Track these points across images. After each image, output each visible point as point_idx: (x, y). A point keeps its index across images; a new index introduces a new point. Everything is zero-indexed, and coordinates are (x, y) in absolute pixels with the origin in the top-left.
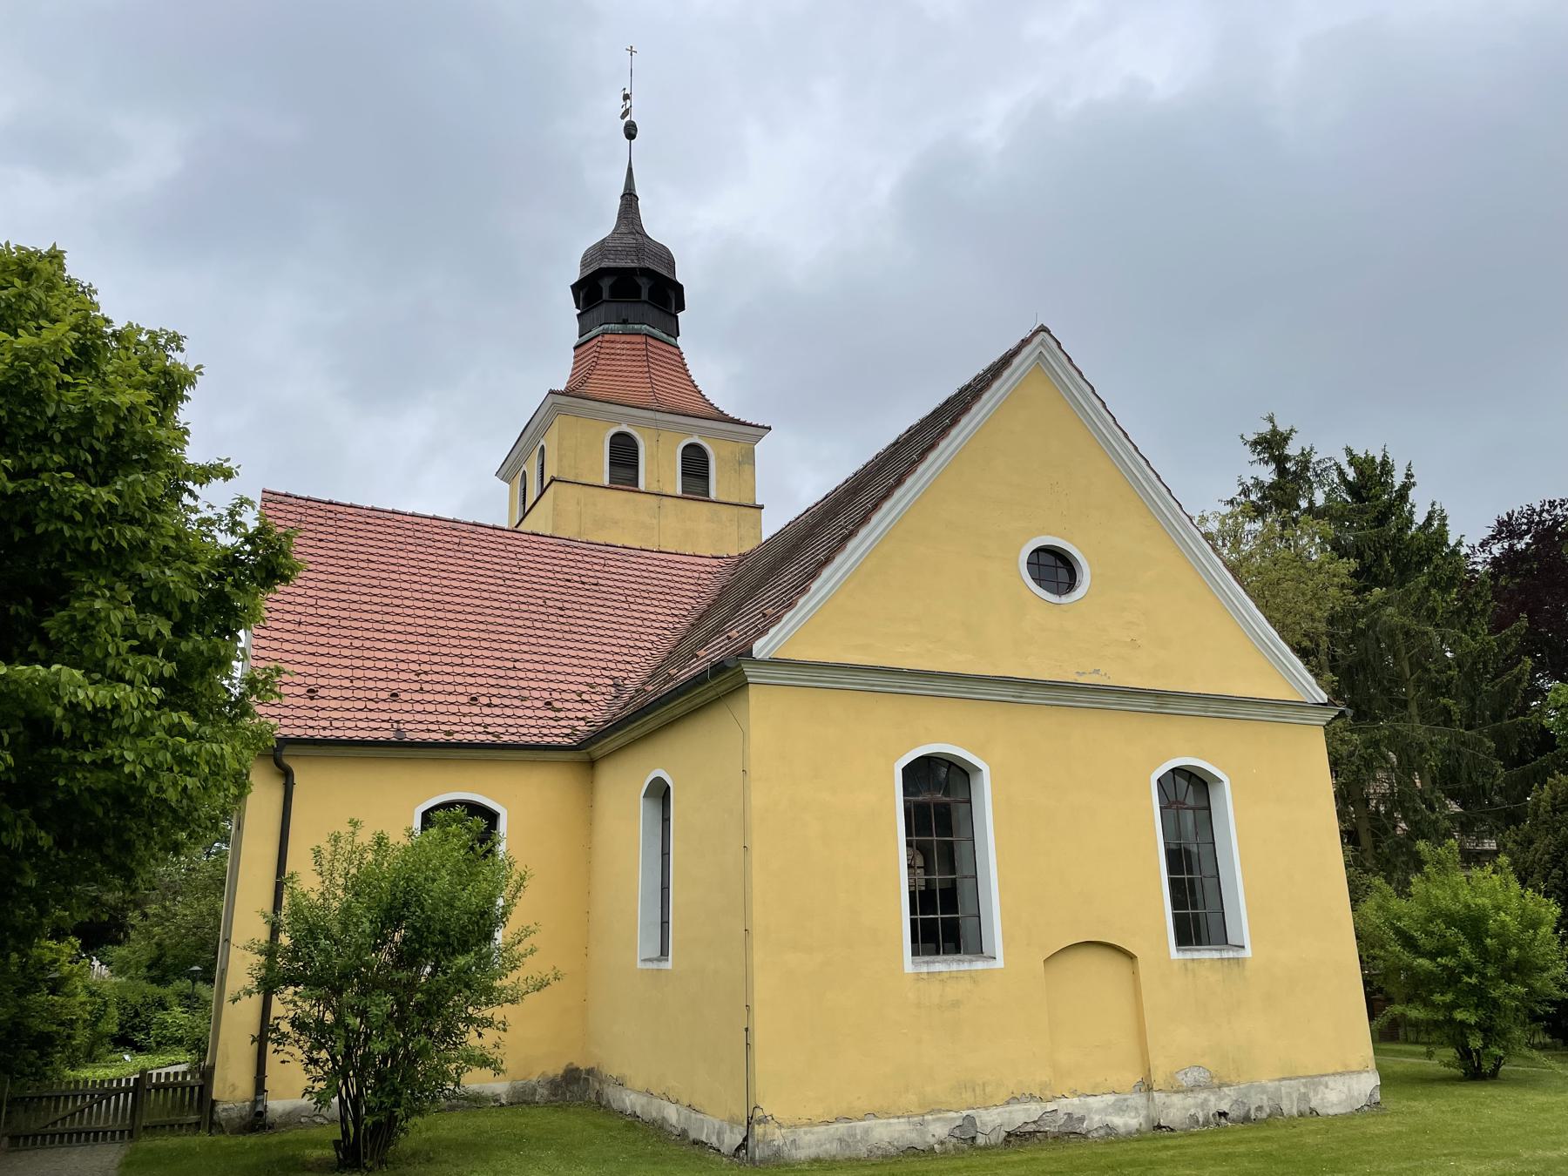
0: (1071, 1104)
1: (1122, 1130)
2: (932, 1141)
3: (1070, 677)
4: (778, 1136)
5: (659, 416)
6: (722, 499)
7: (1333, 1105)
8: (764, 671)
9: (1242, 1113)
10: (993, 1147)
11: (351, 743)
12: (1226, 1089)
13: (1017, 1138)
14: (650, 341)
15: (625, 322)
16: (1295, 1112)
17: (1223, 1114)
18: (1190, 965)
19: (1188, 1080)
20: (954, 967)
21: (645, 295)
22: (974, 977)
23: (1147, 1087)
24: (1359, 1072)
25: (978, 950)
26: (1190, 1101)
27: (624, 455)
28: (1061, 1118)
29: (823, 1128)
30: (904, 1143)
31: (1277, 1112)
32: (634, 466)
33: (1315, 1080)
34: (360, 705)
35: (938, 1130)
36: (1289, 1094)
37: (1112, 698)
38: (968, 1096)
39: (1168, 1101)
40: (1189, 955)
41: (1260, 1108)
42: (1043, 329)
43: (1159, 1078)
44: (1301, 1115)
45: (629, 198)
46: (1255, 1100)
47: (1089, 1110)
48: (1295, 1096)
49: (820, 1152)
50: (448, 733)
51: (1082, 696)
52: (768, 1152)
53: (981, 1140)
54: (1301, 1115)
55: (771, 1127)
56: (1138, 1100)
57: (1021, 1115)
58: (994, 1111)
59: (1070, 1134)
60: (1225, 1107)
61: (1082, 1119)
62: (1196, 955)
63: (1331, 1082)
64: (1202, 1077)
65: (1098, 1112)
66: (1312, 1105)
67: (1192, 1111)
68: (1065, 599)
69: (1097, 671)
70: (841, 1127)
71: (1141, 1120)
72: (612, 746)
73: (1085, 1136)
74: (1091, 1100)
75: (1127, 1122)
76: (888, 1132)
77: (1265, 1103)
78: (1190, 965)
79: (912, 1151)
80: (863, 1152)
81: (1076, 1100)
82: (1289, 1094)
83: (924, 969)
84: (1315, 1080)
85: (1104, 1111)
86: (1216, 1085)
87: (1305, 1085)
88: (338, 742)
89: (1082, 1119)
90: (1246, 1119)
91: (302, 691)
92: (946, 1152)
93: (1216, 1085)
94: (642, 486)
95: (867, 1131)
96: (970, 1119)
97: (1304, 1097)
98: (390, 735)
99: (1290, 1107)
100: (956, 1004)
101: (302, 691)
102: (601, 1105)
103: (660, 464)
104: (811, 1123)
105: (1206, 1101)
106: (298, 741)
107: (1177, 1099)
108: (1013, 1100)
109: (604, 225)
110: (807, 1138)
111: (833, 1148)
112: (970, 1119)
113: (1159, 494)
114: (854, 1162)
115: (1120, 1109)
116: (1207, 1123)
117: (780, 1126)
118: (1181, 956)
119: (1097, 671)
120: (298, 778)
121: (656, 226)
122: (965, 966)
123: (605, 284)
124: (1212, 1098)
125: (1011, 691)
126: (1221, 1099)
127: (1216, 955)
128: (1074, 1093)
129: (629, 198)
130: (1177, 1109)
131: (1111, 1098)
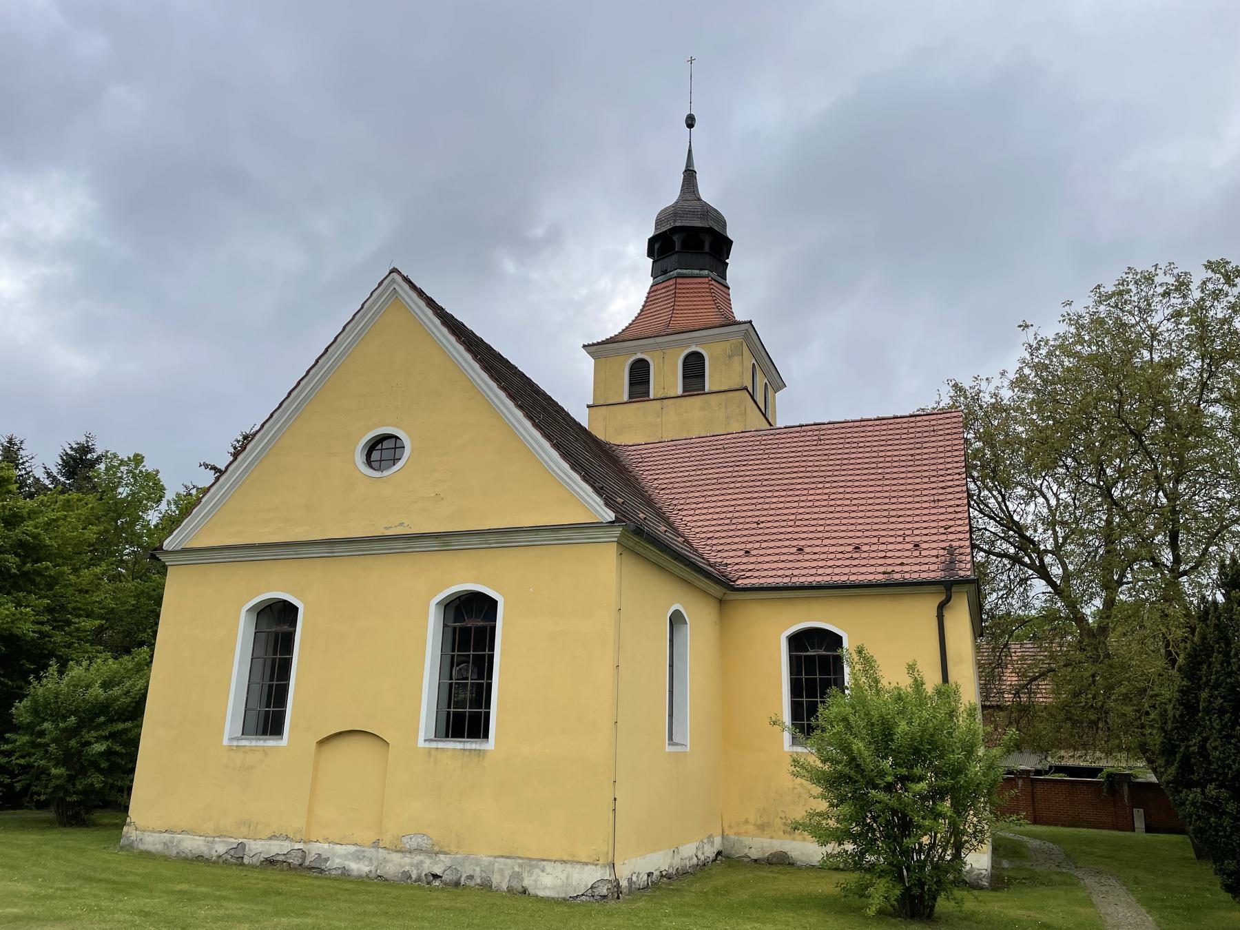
0: (322, 848)
1: (355, 873)
5: (658, 340)
6: (716, 389)
8: (171, 557)
12: (442, 857)
13: (271, 862)
14: (679, 280)
15: (665, 272)
16: (504, 886)
17: (436, 876)
19: (413, 844)
20: (254, 743)
21: (707, 249)
22: (265, 751)
23: (376, 844)
24: (587, 864)
25: (486, 736)
26: (407, 860)
27: (694, 369)
30: (197, 852)
31: (486, 886)
32: (647, 382)
33: (532, 863)
35: (221, 848)
36: (502, 871)
38: (244, 830)
39: (388, 857)
41: (471, 877)
42: (394, 270)
43: (387, 841)
45: (690, 175)
46: (467, 870)
47: (334, 854)
48: (507, 873)
51: (417, 543)
53: (246, 861)
54: (510, 890)
57: (276, 848)
58: (259, 843)
60: (438, 871)
61: (327, 860)
63: (549, 867)
64: (425, 843)
65: (340, 856)
66: (525, 883)
67: (407, 868)
69: (401, 524)
71: (373, 869)
72: (702, 585)
73: (321, 871)
75: (359, 867)
76: (192, 844)
77: (477, 874)
78: (433, 753)
79: (199, 858)
81: (326, 846)
82: (502, 871)
84: (532, 863)
85: (345, 857)
86: (432, 852)
87: (520, 866)
89: (327, 860)
90: (457, 884)
91: (794, 550)
93: (433, 852)
94: (651, 397)
96: (242, 845)
97: (518, 876)
99: (501, 881)
100: (251, 768)
101: (794, 550)
102: (792, 864)
103: (667, 375)
104: (153, 831)
107: (396, 857)
109: (670, 195)
111: (160, 847)
112: (242, 845)
115: (358, 857)
116: (419, 879)
119: (401, 524)
121: (708, 193)
124: (428, 862)
125: (323, 550)
126: (436, 863)
128: (326, 840)
129: (690, 175)
131: (352, 849)
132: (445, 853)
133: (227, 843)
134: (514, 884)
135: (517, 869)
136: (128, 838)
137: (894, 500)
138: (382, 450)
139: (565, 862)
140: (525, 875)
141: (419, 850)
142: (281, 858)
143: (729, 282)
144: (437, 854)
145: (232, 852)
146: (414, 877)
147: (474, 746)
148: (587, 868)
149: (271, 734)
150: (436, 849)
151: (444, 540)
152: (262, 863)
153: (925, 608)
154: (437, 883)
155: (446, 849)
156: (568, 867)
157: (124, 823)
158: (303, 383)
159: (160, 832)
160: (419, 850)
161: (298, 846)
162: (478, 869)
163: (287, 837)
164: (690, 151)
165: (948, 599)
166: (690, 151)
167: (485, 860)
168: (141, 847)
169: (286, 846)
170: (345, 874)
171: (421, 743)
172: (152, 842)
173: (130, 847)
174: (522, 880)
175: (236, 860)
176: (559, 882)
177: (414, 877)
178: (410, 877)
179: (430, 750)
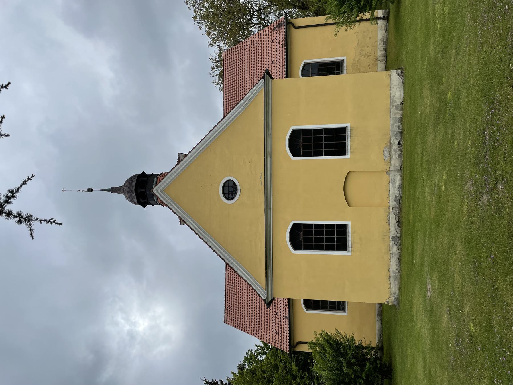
0: (391, 199)
1: (400, 182)
2: (397, 252)
3: (263, 187)
4: (393, 298)
7: (400, 95)
8: (270, 294)
9: (399, 134)
10: (401, 231)
11: (290, 327)
12: (392, 141)
13: (399, 223)
16: (401, 112)
17: (399, 143)
18: (352, 151)
19: (387, 155)
20: (350, 239)
21: (144, 190)
23: (388, 172)
24: (391, 79)
28: (395, 204)
29: (391, 285)
30: (397, 261)
31: (401, 119)
33: (392, 102)
34: (280, 323)
35: (395, 249)
36: (395, 114)
37: (269, 174)
39: (393, 165)
40: (349, 151)
41: (399, 127)
43: (386, 168)
44: (402, 109)
45: (113, 190)
46: (396, 129)
48: (396, 111)
49: (397, 287)
50: (286, 305)
52: (396, 302)
53: (399, 235)
54: (402, 109)
55: (390, 301)
56: (392, 174)
57: (393, 221)
59: (400, 201)
60: (397, 142)
61: (396, 196)
62: (349, 148)
63: (393, 94)
64: (387, 150)
65: (394, 191)
66: (399, 103)
67: (397, 156)
68: (239, 188)
70: (392, 279)
71: (398, 174)
73: (401, 198)
74: (391, 192)
75: (398, 178)
76: (394, 266)
78: (352, 151)
80: (398, 274)
81: (390, 198)
82: (395, 114)
83: (350, 249)
84: (392, 102)
85: (394, 187)
86: (390, 147)
87: (393, 106)
88: (290, 330)
89: (396, 196)
90: (401, 133)
92: (401, 249)
95: (393, 272)
97: (397, 106)
98: (287, 321)
99: (398, 114)
101: (277, 311)
104: (390, 288)
105: (394, 150)
106: (290, 342)
107: (393, 161)
108: (388, 223)
109: (121, 198)
110: (393, 290)
111: (397, 283)
112: (393, 238)
113: (199, 148)
114: (401, 277)
115: (394, 182)
116: (401, 150)
117: (390, 297)
118: (349, 154)
120: (299, 340)
121: (121, 183)
122: (350, 235)
123: (142, 201)
125: (269, 213)
126: (394, 143)
127: (349, 139)
128: (388, 198)
129: (113, 190)
130: (396, 162)
131: (391, 185)
132: (390, 140)
133: (392, 246)
134: (400, 108)
135: (394, 107)
136: (394, 301)
137: (255, 60)
138: (230, 190)
139: (390, 87)
140: (396, 104)
141: (390, 152)
142: (397, 216)
143: (160, 173)
144: (391, 144)
145: (396, 243)
146: (400, 153)
147: (349, 133)
148: (392, 79)
149: (346, 229)
150: (389, 144)
151: (268, 154)
152: (400, 227)
153: (296, 34)
154: (401, 142)
155: (389, 140)
156: (392, 86)
157: (388, 305)
158: (197, 232)
159: (390, 283)
160: (390, 152)
161: (391, 210)
162: (395, 125)
163: (388, 216)
164: (103, 190)
165: (292, 24)
166: (103, 190)
167: (392, 122)
168: (397, 292)
169: (392, 216)
170: (401, 187)
171: (346, 314)
172: (394, 288)
173: (398, 300)
174: (398, 105)
175: (398, 240)
176: (398, 89)
177: (400, 153)
178: (400, 154)
179: (351, 152)
